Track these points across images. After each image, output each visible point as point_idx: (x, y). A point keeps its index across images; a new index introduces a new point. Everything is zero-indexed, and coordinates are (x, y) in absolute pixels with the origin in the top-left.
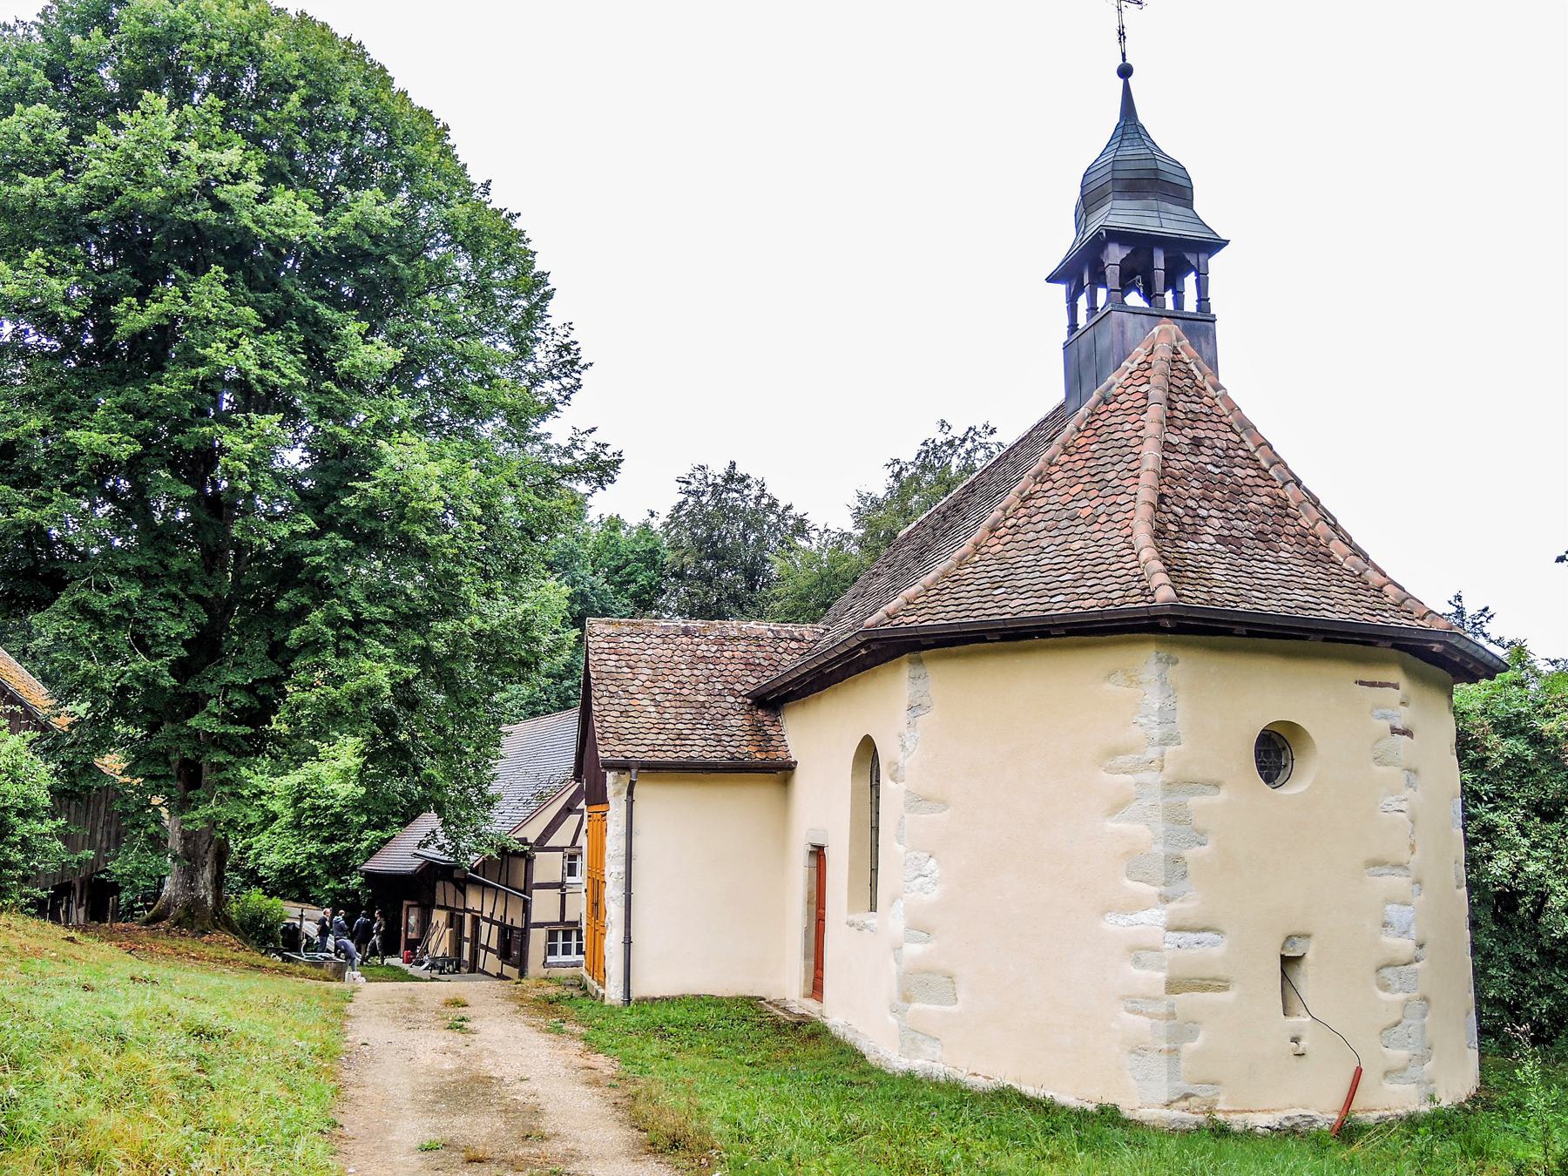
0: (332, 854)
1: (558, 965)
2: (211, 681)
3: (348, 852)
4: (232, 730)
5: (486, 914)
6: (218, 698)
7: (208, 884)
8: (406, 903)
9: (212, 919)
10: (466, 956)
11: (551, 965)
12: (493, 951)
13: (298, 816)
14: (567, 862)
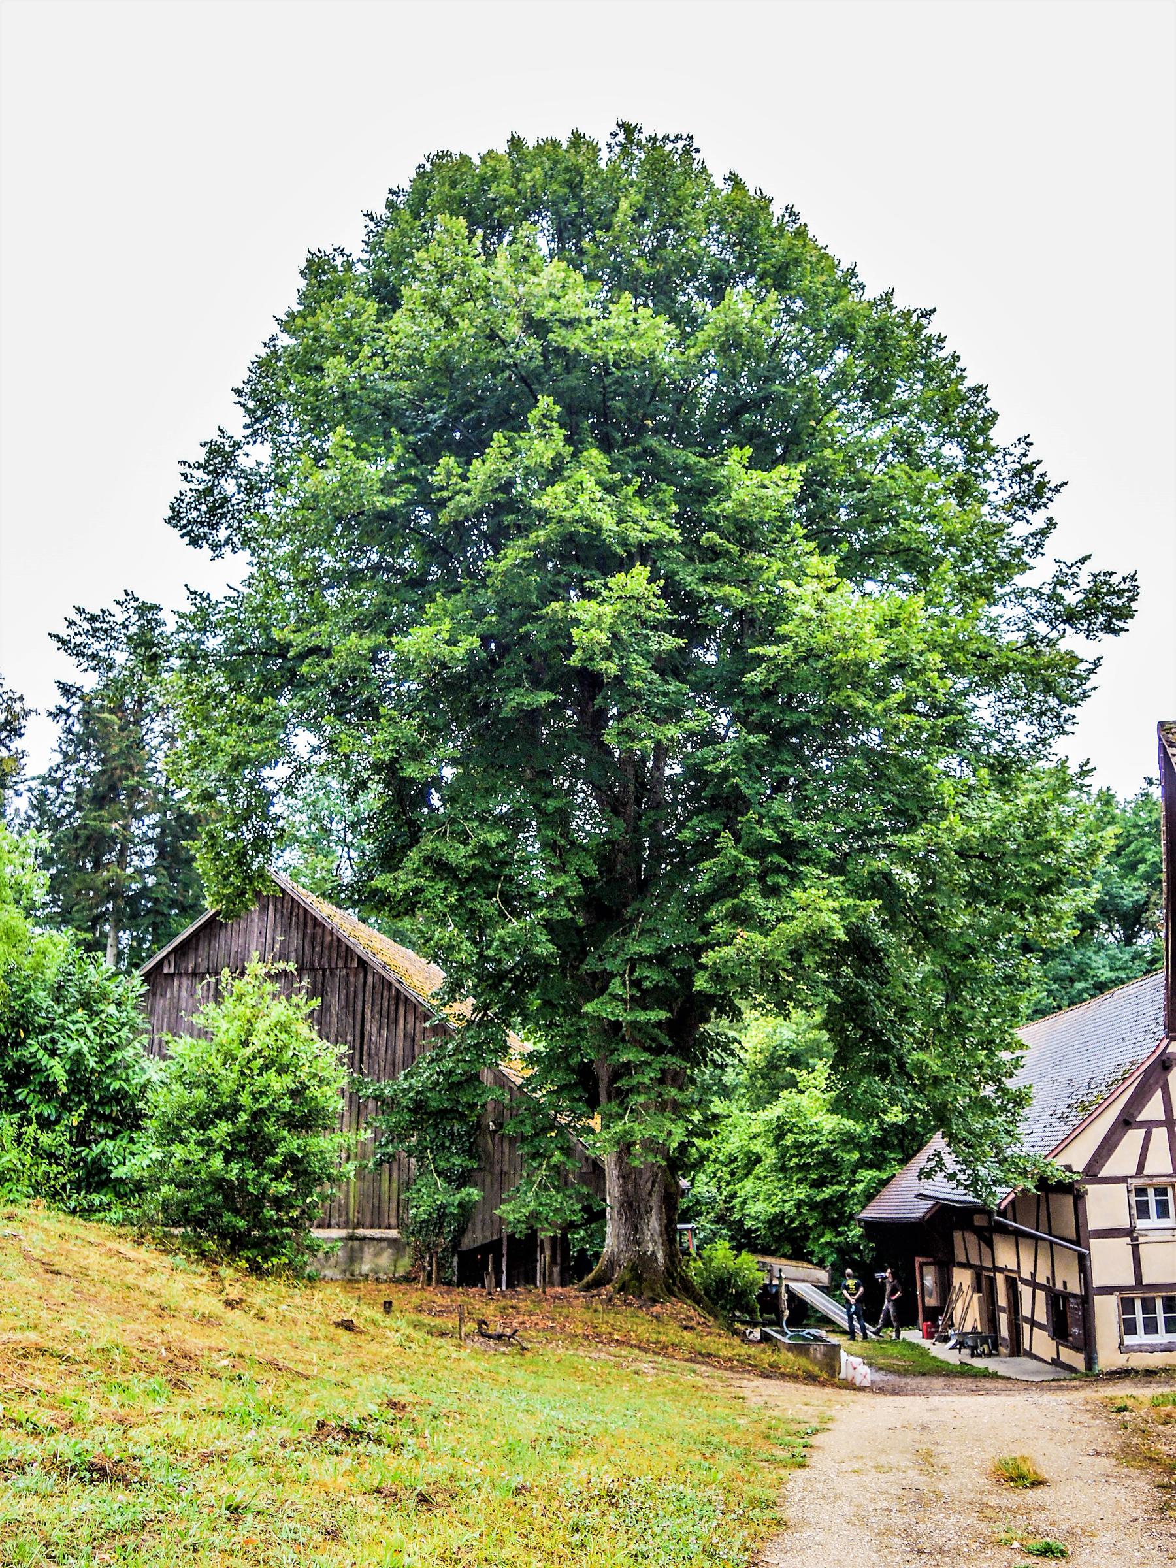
0: (824, 1200)
1: (1141, 1349)
2: (614, 956)
3: (843, 1197)
4: (642, 1017)
5: (1026, 1274)
6: (622, 976)
7: (656, 1237)
8: (918, 1260)
9: (666, 1283)
10: (1004, 1332)
11: (1130, 1349)
12: (1041, 1327)
13: (782, 1157)
14: (1133, 1199)
